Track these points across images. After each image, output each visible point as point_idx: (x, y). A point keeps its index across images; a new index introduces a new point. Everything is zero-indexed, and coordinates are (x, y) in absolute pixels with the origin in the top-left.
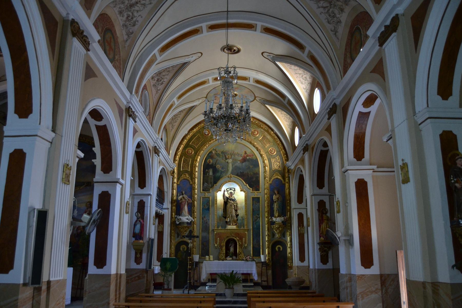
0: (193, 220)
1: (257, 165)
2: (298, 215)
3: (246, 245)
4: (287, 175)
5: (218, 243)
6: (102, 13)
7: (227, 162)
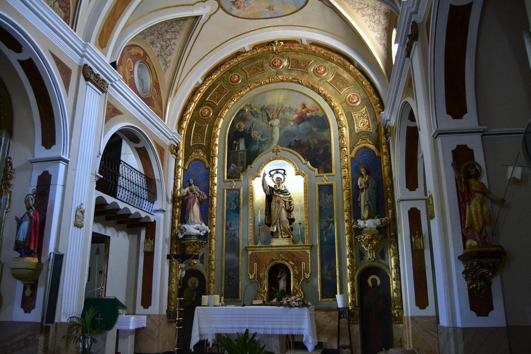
0: (209, 231)
3: (309, 275)
4: (383, 140)
7: (271, 125)
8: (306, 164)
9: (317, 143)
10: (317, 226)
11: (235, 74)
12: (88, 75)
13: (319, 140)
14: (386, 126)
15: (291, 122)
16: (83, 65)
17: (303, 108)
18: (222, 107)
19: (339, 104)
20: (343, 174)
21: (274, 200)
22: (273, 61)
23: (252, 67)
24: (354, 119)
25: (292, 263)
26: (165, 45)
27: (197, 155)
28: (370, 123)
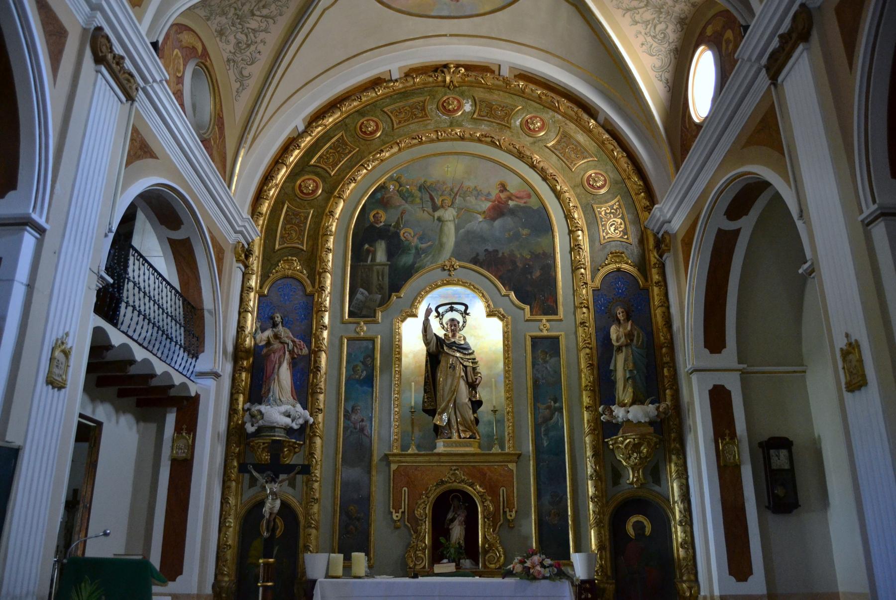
0: (311, 420)
1: (544, 226)
2: (711, 392)
3: (513, 514)
4: (653, 257)
5: (404, 506)
6: (176, 22)
7: (439, 219)
8: (508, 296)
9: (528, 257)
10: (529, 416)
11: (370, 120)
12: (102, 52)
13: (532, 253)
14: (658, 233)
15: (479, 216)
16: (93, 28)
17: (501, 191)
18: (343, 179)
19: (571, 189)
20: (580, 317)
21: (443, 363)
22: (444, 101)
23: (403, 108)
24: (599, 218)
25: (481, 490)
26: (245, 42)
27: (287, 267)
28: (628, 226)
